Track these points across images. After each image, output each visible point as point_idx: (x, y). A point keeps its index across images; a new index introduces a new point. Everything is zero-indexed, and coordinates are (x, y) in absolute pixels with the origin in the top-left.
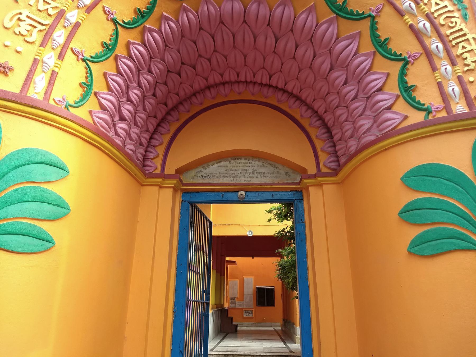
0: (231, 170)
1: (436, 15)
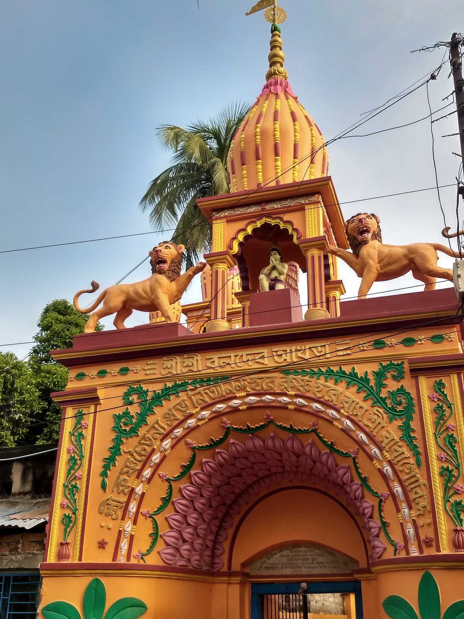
0: (293, 560)
1: (395, 461)
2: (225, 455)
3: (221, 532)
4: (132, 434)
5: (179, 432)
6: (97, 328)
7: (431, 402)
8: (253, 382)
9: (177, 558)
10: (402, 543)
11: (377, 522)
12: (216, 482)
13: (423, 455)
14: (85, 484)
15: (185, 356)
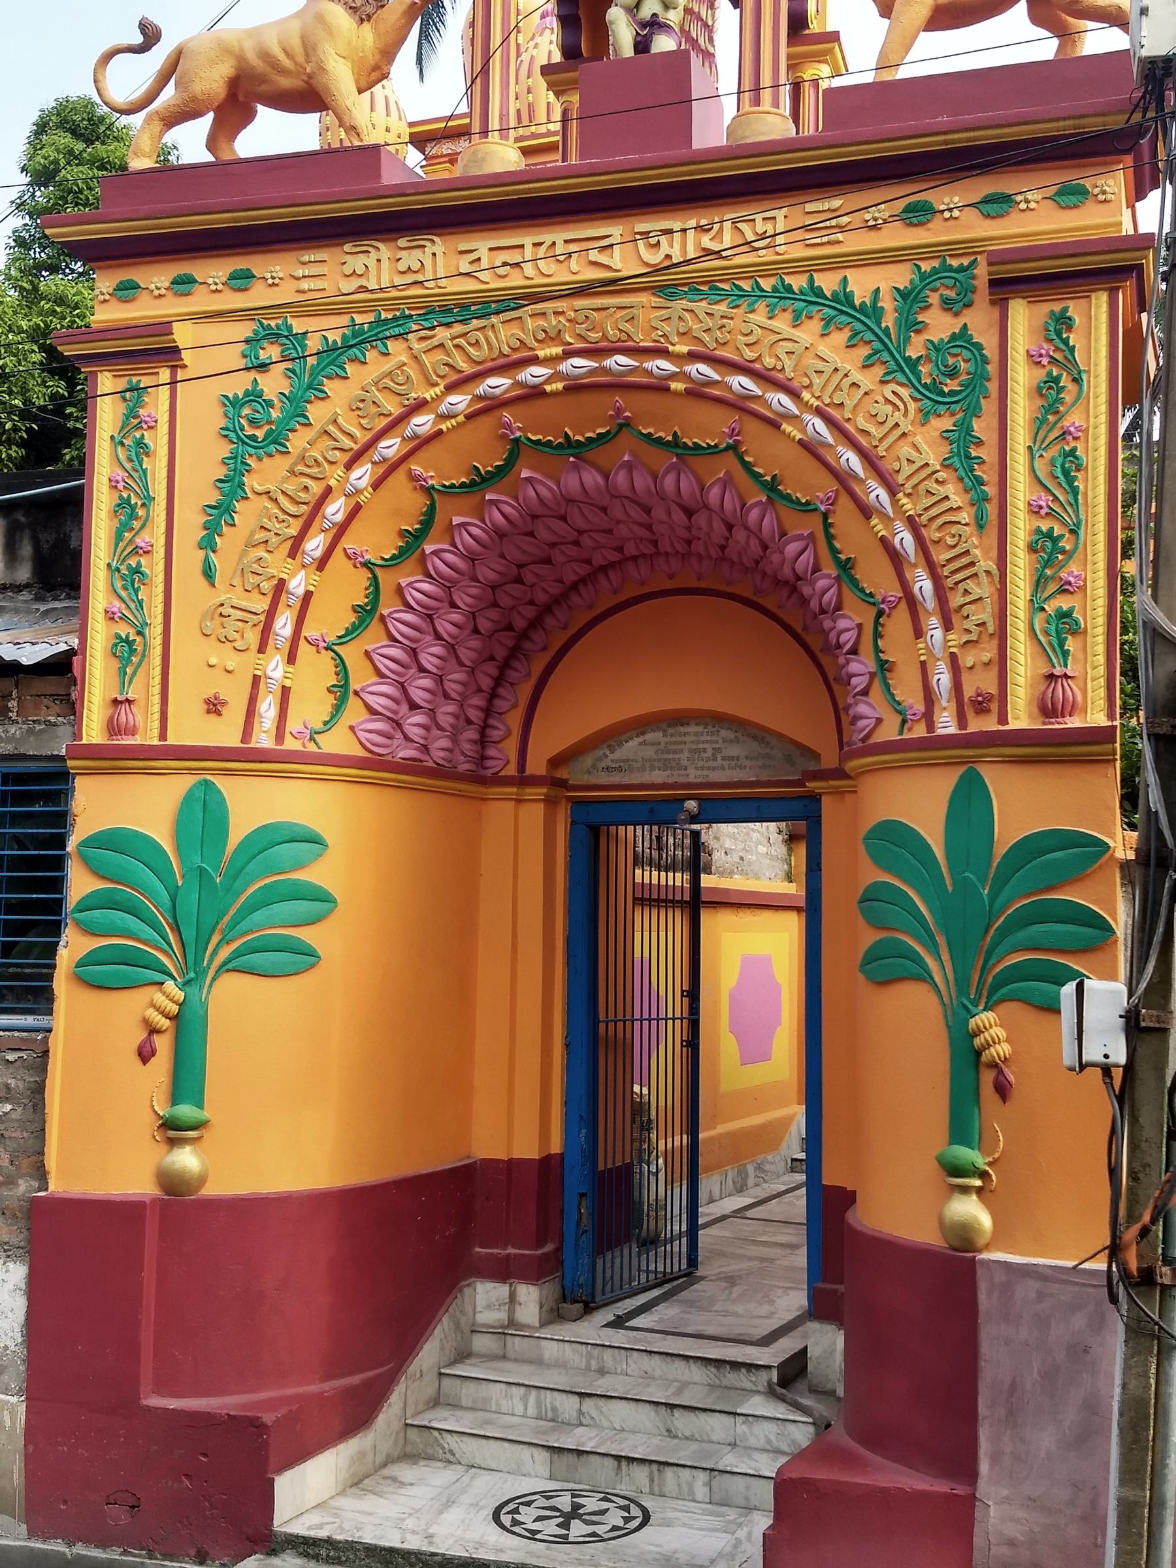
1: (924, 519)
2: (507, 509)
3: (502, 691)
4: (272, 448)
5: (391, 447)
6: (165, 152)
7: (1033, 366)
8: (581, 318)
9: (396, 742)
10: (920, 707)
11: (866, 661)
12: (486, 573)
13: (995, 501)
14: (161, 566)
15: (402, 242)
